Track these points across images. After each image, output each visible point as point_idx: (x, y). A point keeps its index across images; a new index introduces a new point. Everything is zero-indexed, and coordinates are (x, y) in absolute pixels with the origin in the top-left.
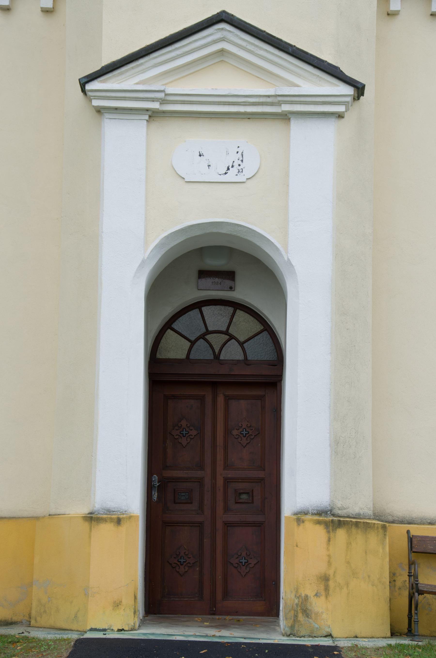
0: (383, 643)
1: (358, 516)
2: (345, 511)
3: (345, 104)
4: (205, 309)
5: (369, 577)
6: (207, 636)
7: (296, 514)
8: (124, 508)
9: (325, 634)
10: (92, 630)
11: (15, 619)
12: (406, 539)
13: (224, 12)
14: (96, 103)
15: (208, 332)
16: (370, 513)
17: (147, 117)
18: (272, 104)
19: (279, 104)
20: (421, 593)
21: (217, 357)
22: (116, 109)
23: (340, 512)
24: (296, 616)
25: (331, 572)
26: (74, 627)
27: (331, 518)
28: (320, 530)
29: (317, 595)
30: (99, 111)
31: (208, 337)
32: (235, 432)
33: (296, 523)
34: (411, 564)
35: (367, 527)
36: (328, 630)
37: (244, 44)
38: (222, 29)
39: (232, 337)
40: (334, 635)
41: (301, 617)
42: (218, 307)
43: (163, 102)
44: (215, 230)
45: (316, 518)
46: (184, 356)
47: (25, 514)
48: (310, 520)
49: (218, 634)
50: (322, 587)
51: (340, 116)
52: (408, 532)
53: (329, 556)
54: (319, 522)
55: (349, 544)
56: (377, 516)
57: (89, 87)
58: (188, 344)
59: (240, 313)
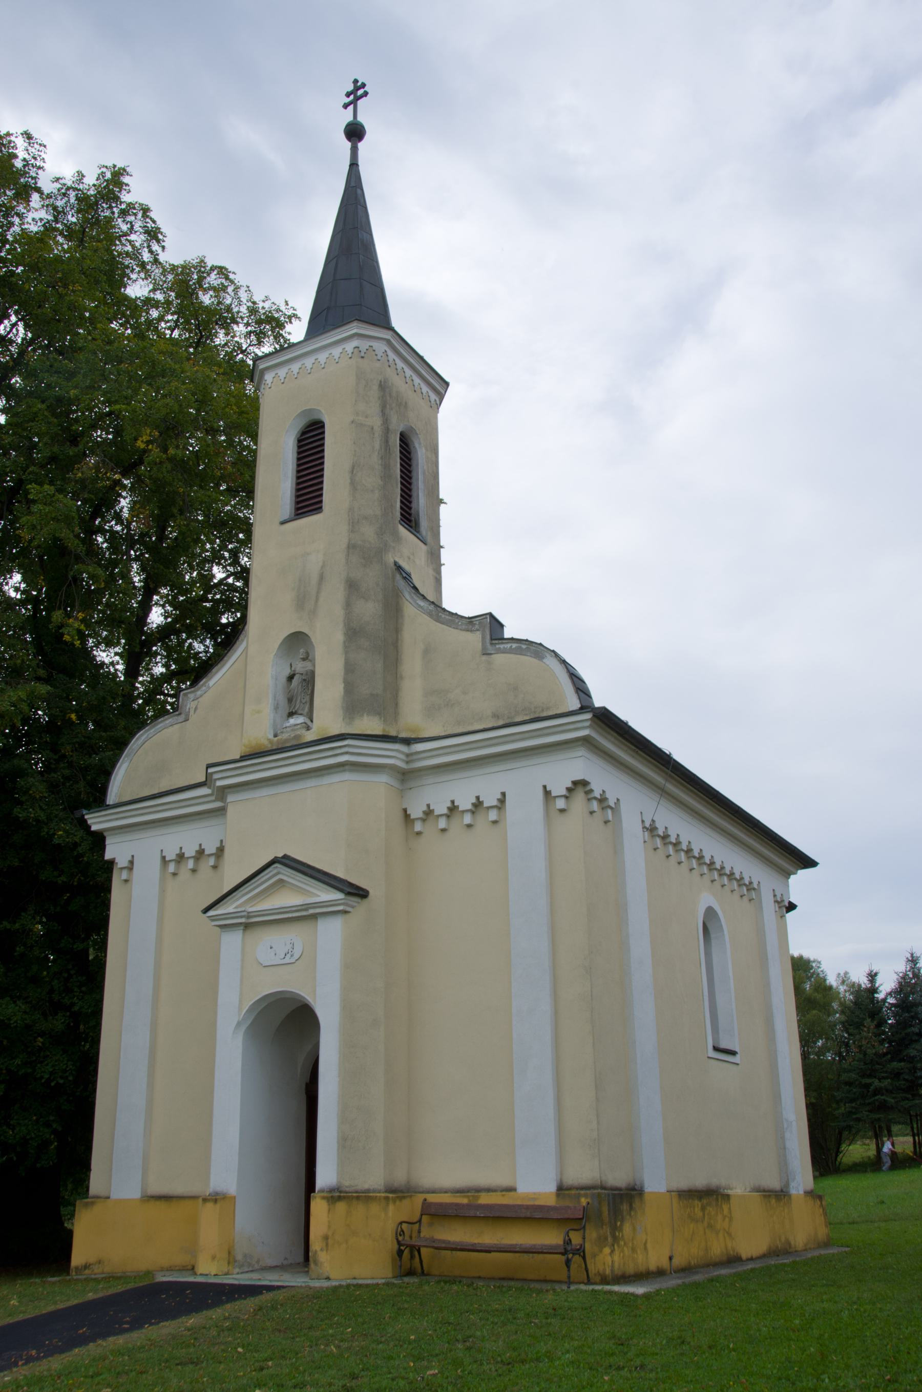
1: (368, 1191)
2: (353, 1188)
5: (370, 1235)
9: (325, 1277)
13: (276, 857)
17: (242, 928)
19: (306, 910)
25: (330, 1234)
29: (322, 1250)
36: (327, 1274)
38: (277, 867)
43: (248, 917)
51: (346, 912)
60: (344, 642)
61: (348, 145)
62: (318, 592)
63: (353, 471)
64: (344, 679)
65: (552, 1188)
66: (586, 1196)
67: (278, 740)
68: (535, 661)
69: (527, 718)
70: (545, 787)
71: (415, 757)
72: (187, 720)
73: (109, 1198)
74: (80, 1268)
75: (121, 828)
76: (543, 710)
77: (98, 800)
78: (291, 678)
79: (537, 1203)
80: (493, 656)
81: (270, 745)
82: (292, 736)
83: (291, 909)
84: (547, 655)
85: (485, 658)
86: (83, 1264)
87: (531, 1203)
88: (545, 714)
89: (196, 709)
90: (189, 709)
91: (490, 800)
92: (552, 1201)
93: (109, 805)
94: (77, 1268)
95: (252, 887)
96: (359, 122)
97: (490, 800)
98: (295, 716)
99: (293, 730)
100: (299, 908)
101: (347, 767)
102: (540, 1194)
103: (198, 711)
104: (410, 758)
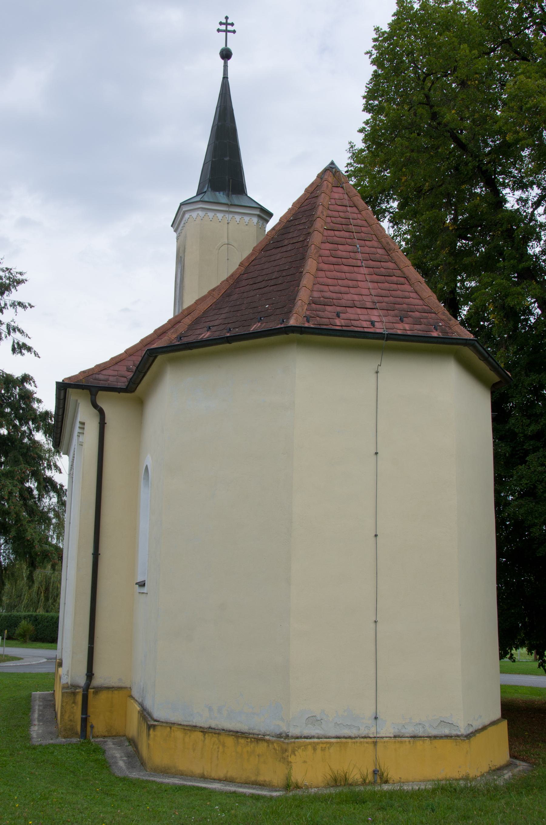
61: (222, 62)
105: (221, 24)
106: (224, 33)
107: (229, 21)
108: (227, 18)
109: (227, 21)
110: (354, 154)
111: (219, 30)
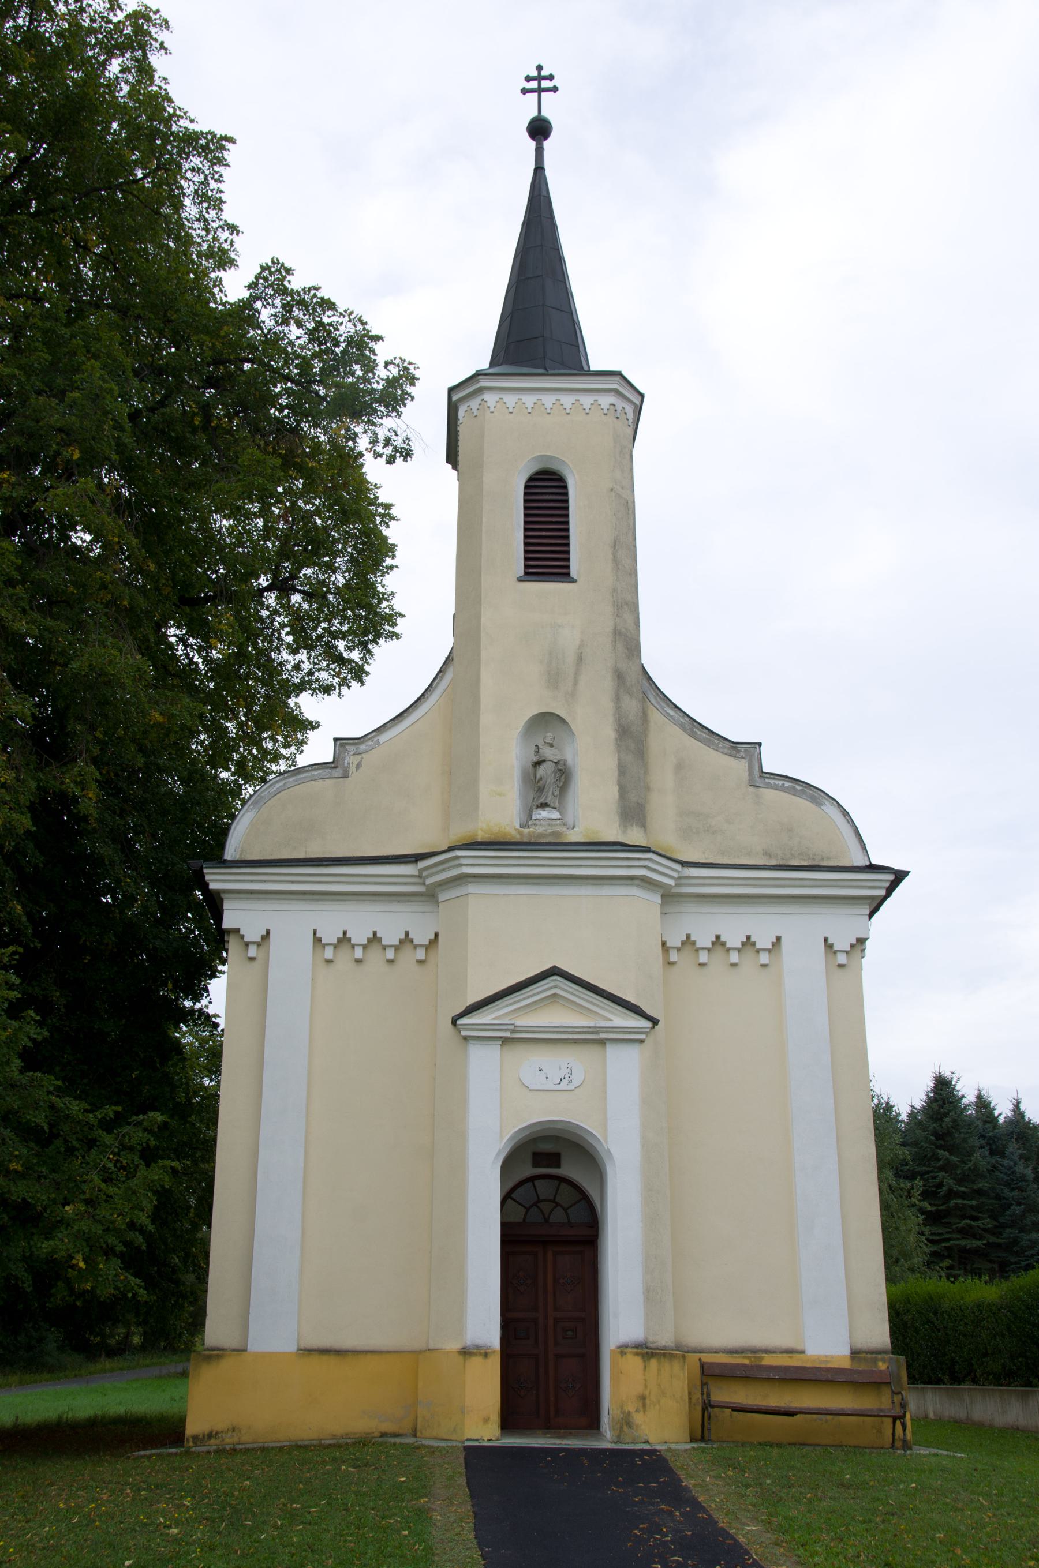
0: (689, 1446)
1: (664, 1348)
3: (647, 1033)
4: (537, 1183)
6: (555, 1444)
7: (619, 1347)
8: (489, 1344)
10: (468, 1440)
11: (401, 1432)
12: (698, 1365)
14: (464, 1033)
15: (539, 1201)
16: (673, 1345)
18: (592, 1033)
19: (598, 1033)
20: (712, 1407)
21: (547, 1221)
22: (478, 1037)
23: (651, 1345)
24: (621, 1428)
25: (647, 1393)
26: (454, 1437)
27: (646, 1350)
28: (638, 1361)
29: (637, 1411)
30: (466, 1038)
31: (539, 1205)
32: (562, 1281)
33: (619, 1355)
34: (703, 1384)
35: (672, 1356)
37: (571, 990)
39: (558, 1204)
40: (650, 1441)
41: (625, 1428)
42: (547, 1180)
43: (512, 1031)
44: (552, 1126)
45: (635, 1350)
46: (521, 1220)
47: (406, 1349)
48: (630, 1353)
49: (563, 1442)
50: (641, 1405)
51: (642, 1041)
52: (700, 1359)
53: (646, 1380)
54: (637, 1354)
55: (659, 1370)
56: (678, 1348)
57: (459, 1022)
58: (524, 1211)
59: (563, 1185)
60: (616, 740)
61: (532, 144)
62: (577, 674)
63: (615, 546)
64: (619, 781)
65: (846, 1351)
66: (883, 1360)
67: (529, 832)
68: (812, 806)
69: (805, 863)
70: (826, 940)
71: (683, 881)
72: (346, 776)
73: (246, 1350)
74: (201, 1436)
75: (251, 893)
76: (823, 859)
77: (215, 853)
78: (537, 764)
79: (829, 1365)
80: (761, 789)
81: (518, 836)
82: (549, 831)
83: (574, 1030)
84: (827, 803)
85: (751, 789)
86: (206, 1433)
87: (823, 1366)
88: (825, 863)
89: (358, 766)
90: (349, 764)
91: (764, 941)
92: (846, 1364)
93: (225, 861)
94: (195, 1438)
95: (519, 998)
96: (544, 117)
97: (764, 941)
98: (547, 809)
99: (549, 825)
100: (585, 1030)
101: (637, 882)
102: (832, 1357)
103: (361, 770)
104: (680, 880)
105: (528, 79)
106: (536, 95)
107: (544, 73)
108: (539, 68)
109: (539, 73)
110: (1018, 1122)
111: (525, 91)
